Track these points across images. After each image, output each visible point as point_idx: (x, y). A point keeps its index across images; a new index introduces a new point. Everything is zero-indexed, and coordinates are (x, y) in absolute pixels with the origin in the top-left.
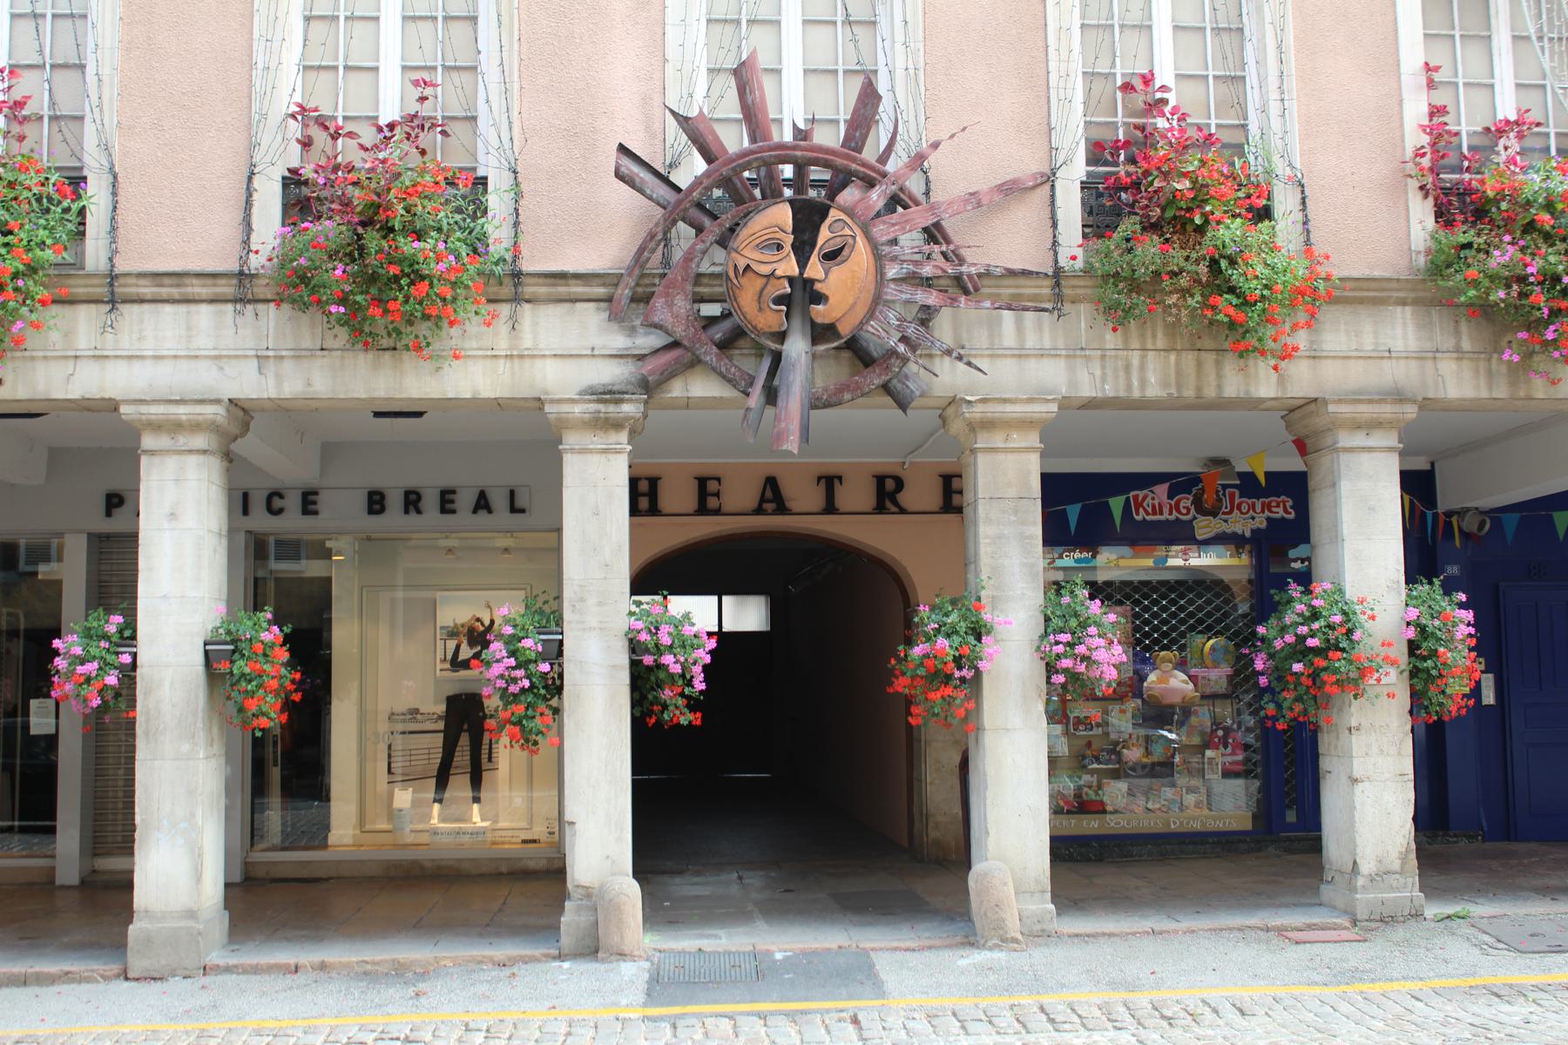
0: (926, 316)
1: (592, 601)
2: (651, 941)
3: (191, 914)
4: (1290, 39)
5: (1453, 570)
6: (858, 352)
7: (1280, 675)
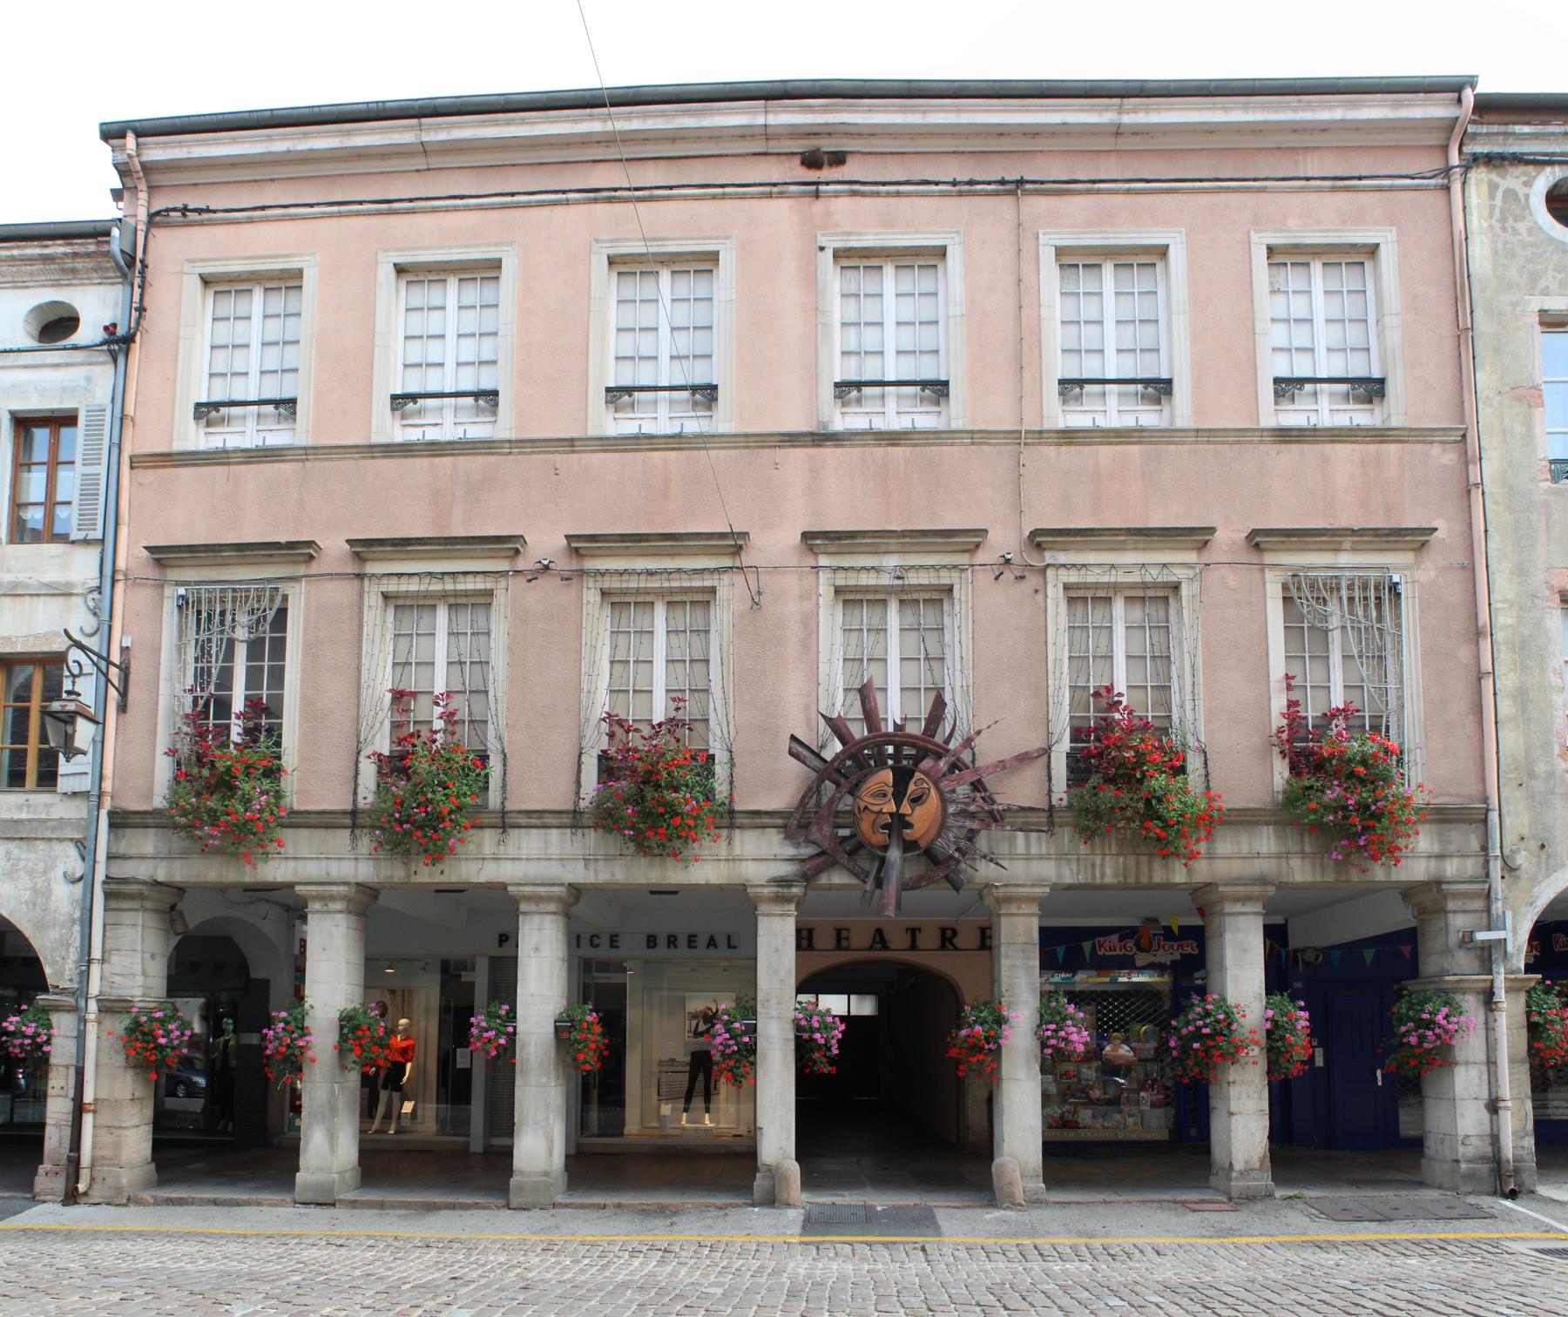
0: (972, 835)
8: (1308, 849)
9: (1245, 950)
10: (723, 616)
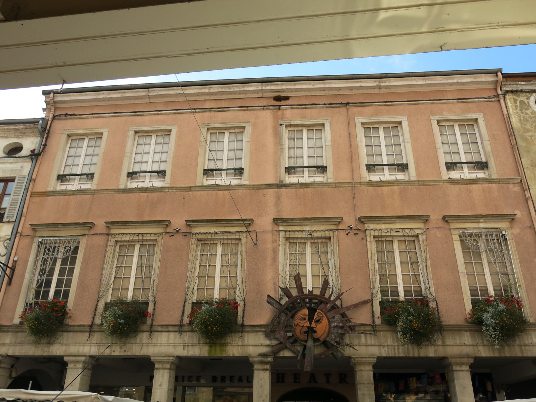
0: (342, 336)
8: (485, 342)
9: (464, 388)
10: (242, 250)
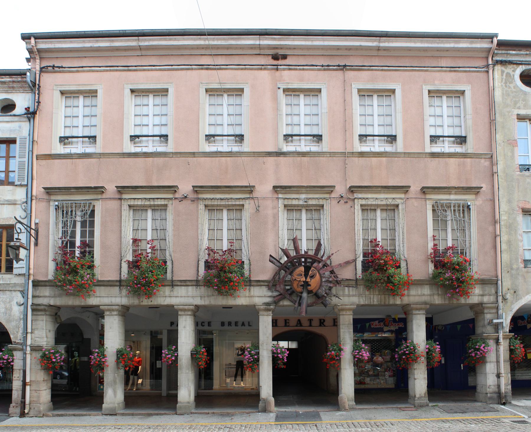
0: (330, 289)
1: (265, 344)
2: (276, 409)
3: (188, 403)
4: (405, 231)
5: (436, 337)
6: (317, 295)
7: (400, 358)
